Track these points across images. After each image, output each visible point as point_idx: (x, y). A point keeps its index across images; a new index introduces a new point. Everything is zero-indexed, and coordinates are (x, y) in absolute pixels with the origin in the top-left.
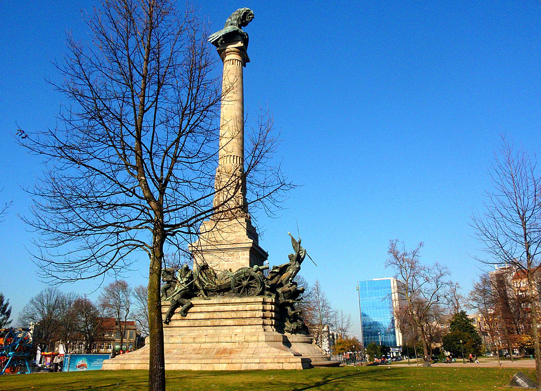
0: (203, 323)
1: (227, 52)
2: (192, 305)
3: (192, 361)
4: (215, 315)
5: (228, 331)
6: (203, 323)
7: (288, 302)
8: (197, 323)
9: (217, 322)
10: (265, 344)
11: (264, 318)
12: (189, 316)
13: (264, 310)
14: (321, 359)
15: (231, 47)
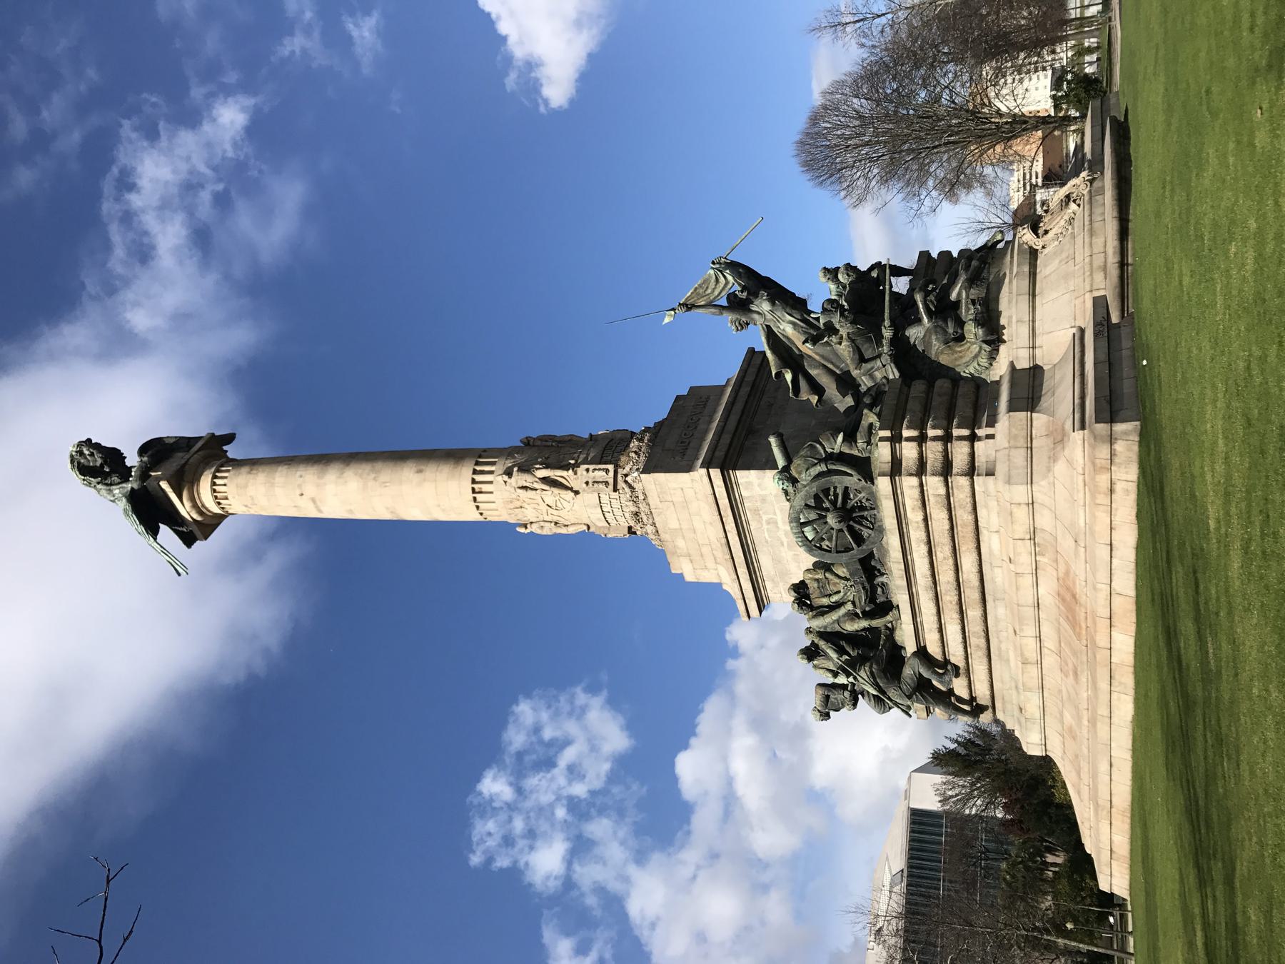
0: (974, 626)
1: (201, 513)
2: (922, 652)
3: (1103, 711)
4: (949, 598)
5: (998, 571)
6: (974, 626)
7: (893, 342)
8: (976, 641)
9: (971, 595)
10: (1041, 486)
11: (946, 470)
12: (956, 656)
13: (921, 470)
14: (1099, 242)
15: (185, 509)
